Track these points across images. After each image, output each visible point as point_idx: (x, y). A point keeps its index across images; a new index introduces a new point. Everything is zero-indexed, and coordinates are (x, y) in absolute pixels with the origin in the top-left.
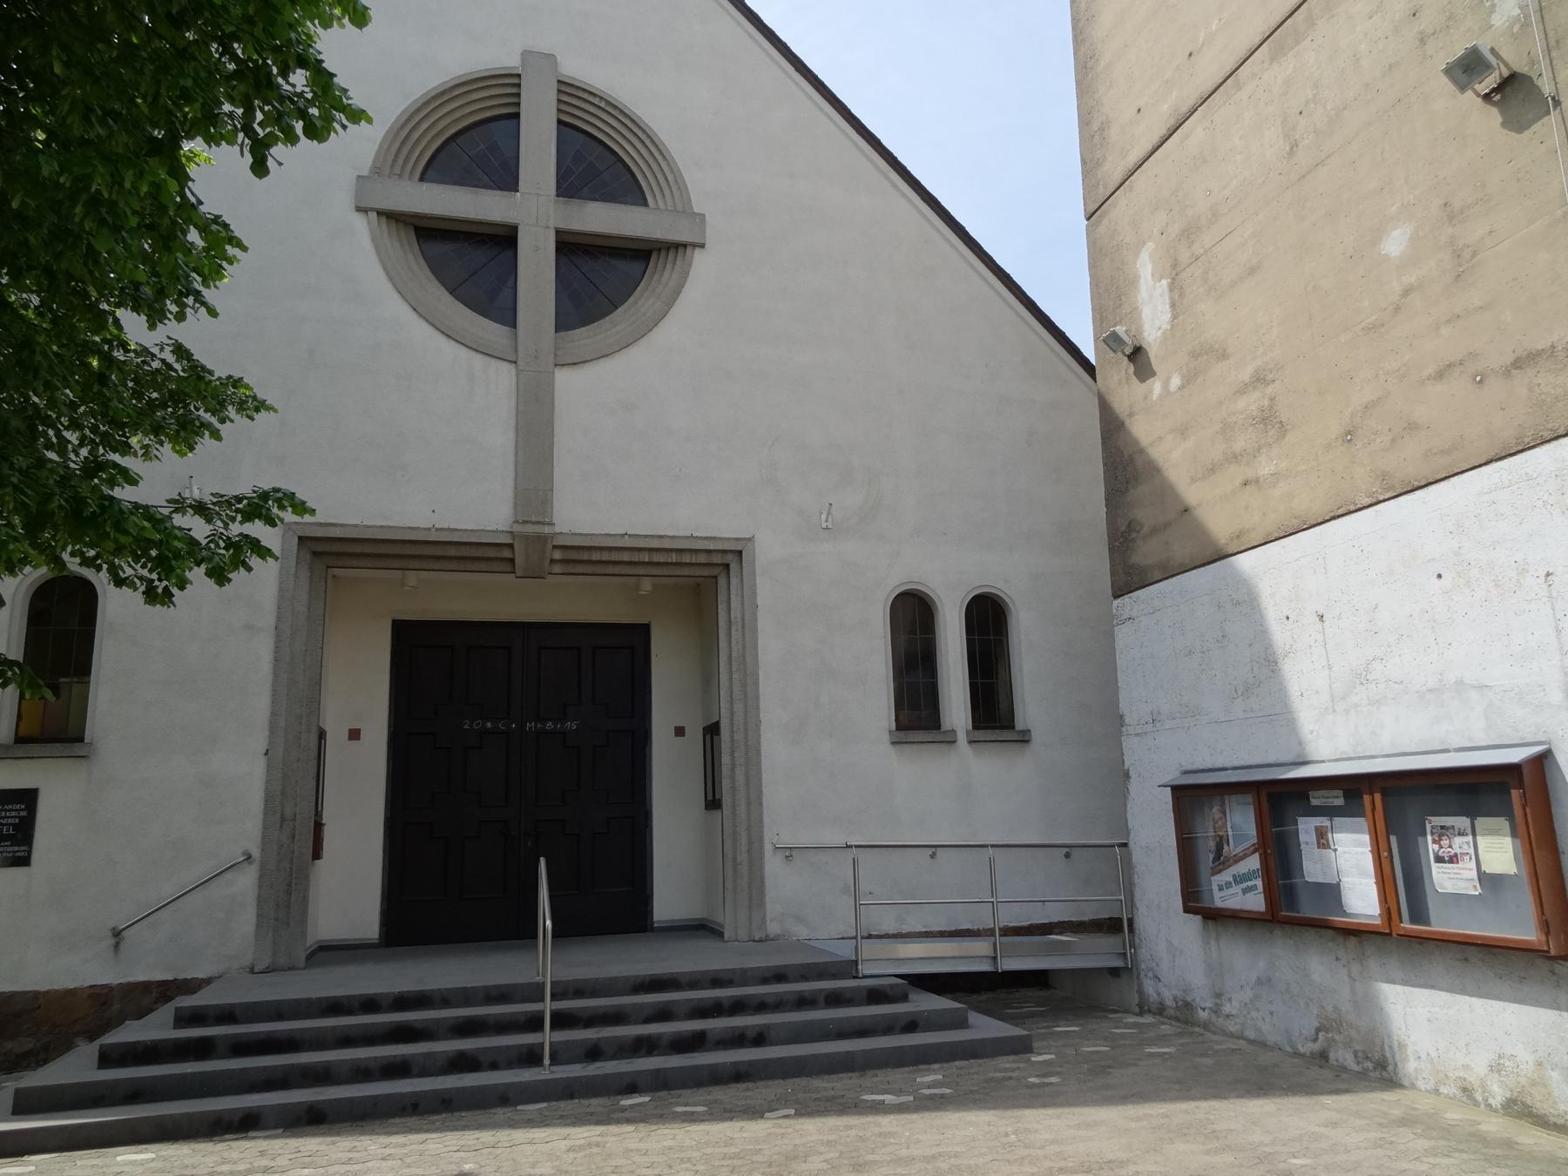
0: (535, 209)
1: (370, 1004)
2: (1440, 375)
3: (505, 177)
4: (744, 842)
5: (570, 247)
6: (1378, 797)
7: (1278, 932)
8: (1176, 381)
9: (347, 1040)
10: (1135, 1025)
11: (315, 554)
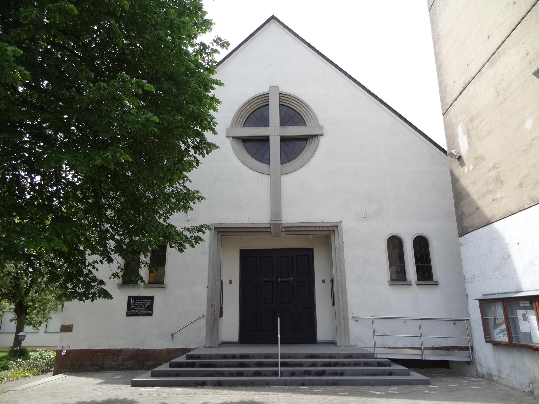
0: (274, 131)
1: (234, 357)
3: (266, 123)
4: (342, 316)
5: (284, 140)
6: (537, 303)
7: (515, 349)
8: (471, 167)
9: (228, 366)
10: (473, 381)
11: (219, 232)
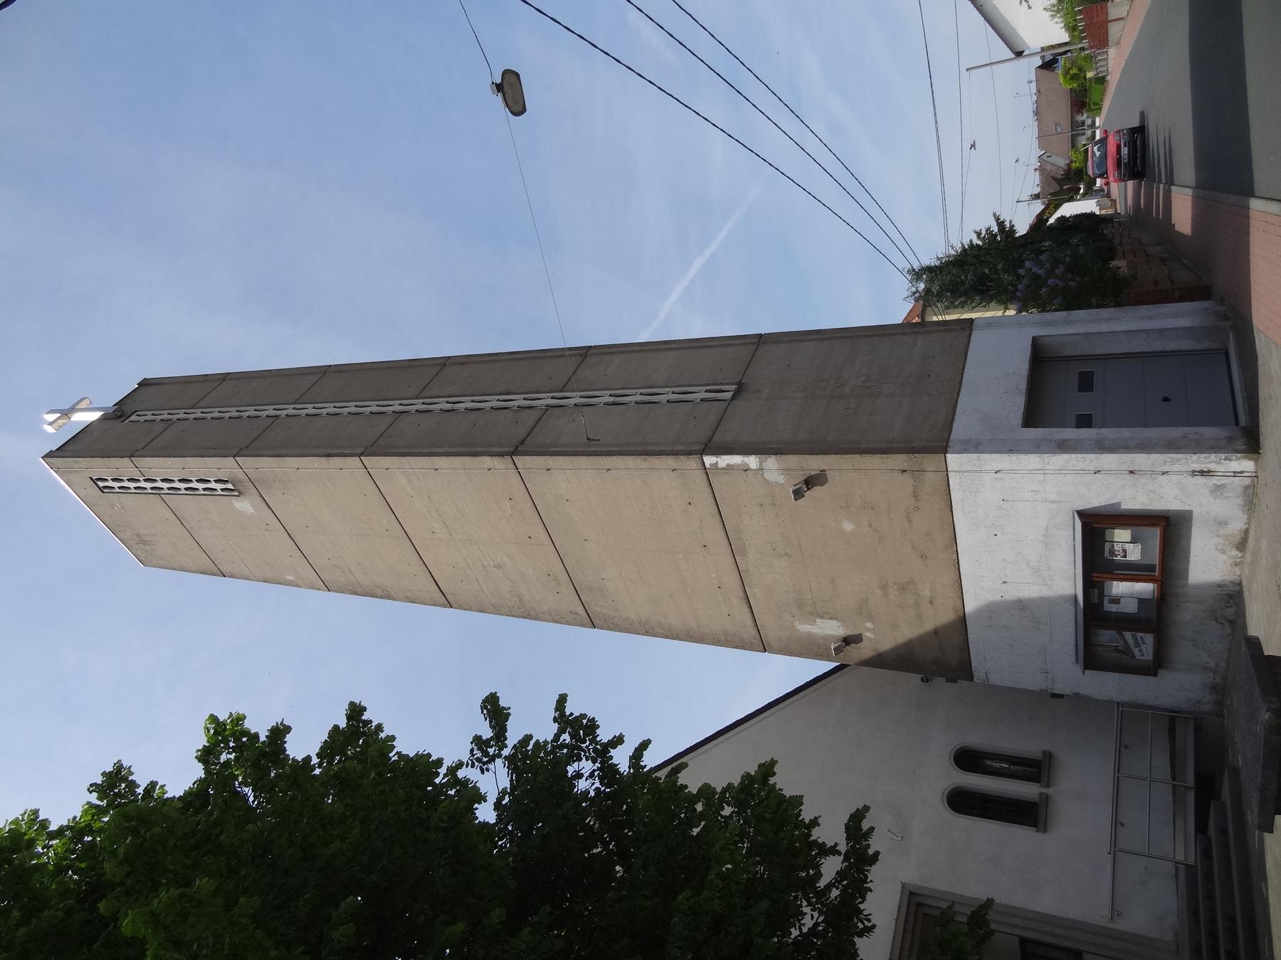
2: (910, 521)
8: (869, 625)
